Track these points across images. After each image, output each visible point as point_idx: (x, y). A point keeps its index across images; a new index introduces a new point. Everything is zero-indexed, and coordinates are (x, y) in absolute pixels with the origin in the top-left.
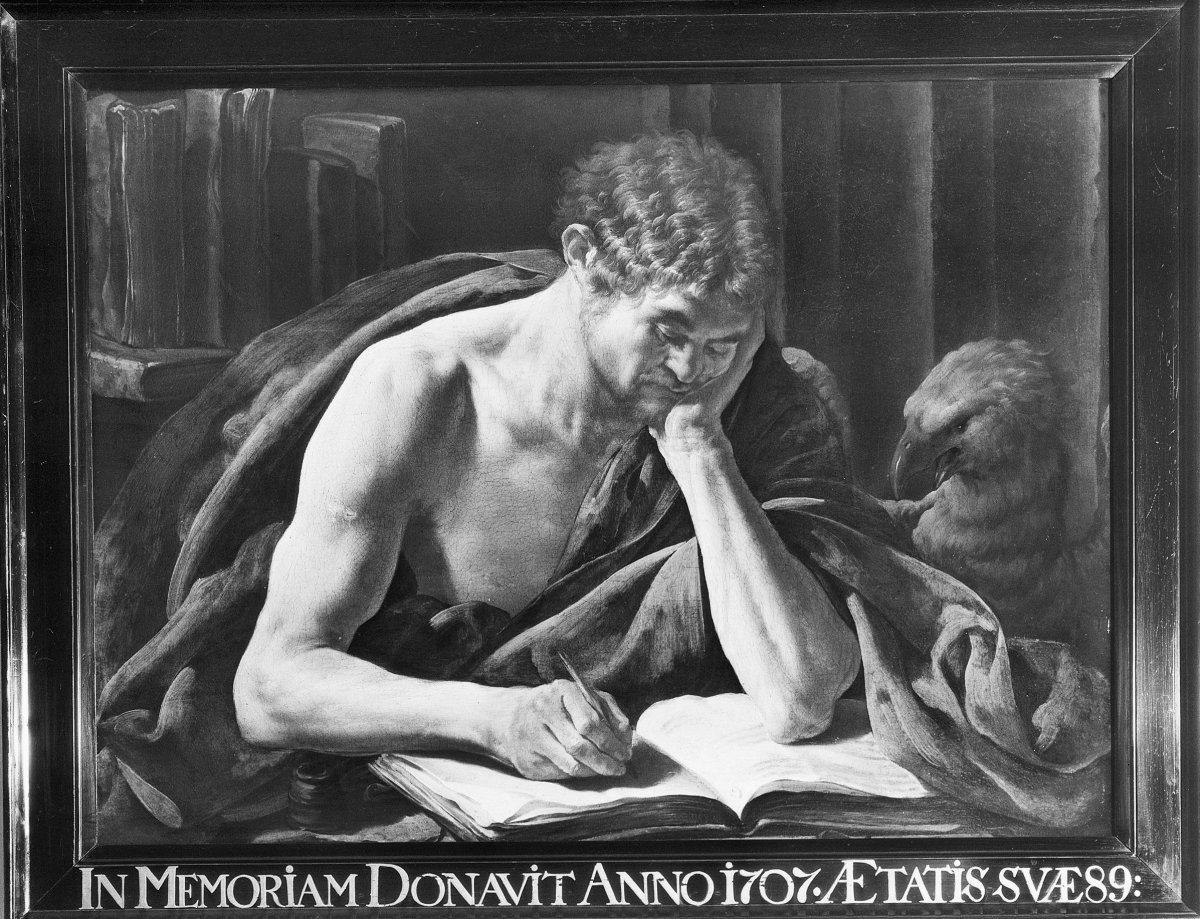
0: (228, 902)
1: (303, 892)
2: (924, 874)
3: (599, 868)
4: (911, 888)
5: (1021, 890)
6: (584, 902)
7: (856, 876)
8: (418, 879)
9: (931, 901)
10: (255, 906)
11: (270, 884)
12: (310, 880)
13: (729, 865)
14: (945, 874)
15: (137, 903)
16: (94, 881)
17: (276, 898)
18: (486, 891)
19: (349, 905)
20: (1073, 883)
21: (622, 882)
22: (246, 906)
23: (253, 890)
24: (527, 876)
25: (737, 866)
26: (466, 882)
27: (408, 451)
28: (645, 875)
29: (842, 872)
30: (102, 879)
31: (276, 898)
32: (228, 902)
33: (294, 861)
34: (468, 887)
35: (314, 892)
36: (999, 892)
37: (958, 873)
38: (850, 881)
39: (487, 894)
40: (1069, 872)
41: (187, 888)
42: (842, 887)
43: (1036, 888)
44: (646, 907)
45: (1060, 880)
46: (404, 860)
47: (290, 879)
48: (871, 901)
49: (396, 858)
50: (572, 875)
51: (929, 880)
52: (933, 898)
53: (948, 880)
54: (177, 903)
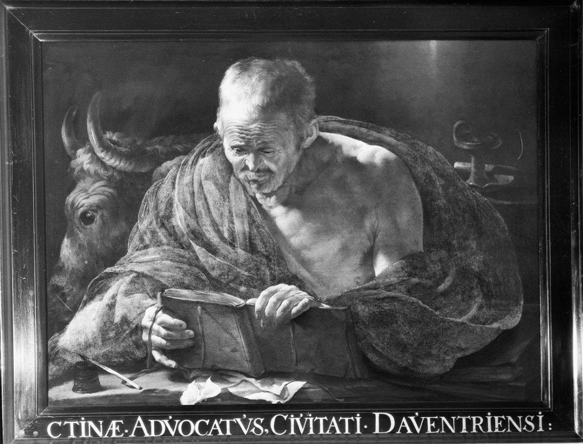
2: (220, 423)
3: (139, 419)
4: (331, 427)
6: (399, 432)
11: (478, 421)
13: (489, 414)
14: (75, 425)
15: (427, 431)
16: (87, 425)
17: (481, 428)
18: (401, 426)
19: (375, 433)
22: (186, 436)
23: (51, 429)
24: (307, 419)
25: (314, 416)
26: (98, 425)
27: (389, 256)
30: (91, 423)
31: (481, 428)
33: (85, 415)
34: (92, 430)
35: (143, 426)
36: (253, 430)
37: (83, 423)
39: (137, 428)
41: (499, 422)
42: (111, 432)
43: (91, 427)
44: (101, 439)
48: (438, 432)
50: (326, 418)
51: (223, 426)
53: (234, 426)
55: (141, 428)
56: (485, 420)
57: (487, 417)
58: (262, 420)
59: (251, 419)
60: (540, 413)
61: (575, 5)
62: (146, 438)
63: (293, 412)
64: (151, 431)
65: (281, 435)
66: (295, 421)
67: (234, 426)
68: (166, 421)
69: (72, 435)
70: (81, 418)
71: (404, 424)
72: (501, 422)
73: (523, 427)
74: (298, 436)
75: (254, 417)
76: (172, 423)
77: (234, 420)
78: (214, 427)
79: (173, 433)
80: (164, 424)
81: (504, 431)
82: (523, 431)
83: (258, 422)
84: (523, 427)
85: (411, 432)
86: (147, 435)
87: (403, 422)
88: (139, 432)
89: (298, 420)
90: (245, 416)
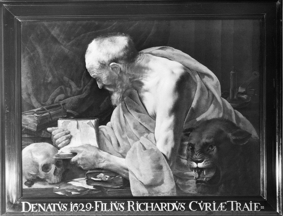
0: (139, 209)
1: (244, 207)
2: (51, 205)
4: (156, 208)
5: (124, 208)
7: (223, 206)
8: (141, 204)
9: (160, 210)
10: (30, 211)
11: (208, 205)
12: (157, 204)
13: (112, 202)
14: (56, 205)
17: (165, 209)
20: (257, 206)
21: (39, 206)
26: (43, 206)
28: (162, 204)
29: (220, 205)
31: (165, 209)
32: (139, 209)
34: (41, 208)
36: (180, 209)
38: (222, 207)
39: (48, 209)
40: (207, 204)
41: (98, 205)
42: (220, 208)
43: (61, 208)
45: (221, 205)
46: (30, 201)
47: (214, 204)
49: (133, 200)
52: (250, 210)
53: (57, 207)
54: (104, 209)
55: (247, 208)
56: (212, 205)
57: (71, 204)
58: (184, 204)
59: (179, 204)
60: (71, 202)
61: (278, 3)
62: (52, 212)
63: (72, 201)
64: (168, 209)
65: (143, 211)
66: (113, 205)
67: (57, 207)
68: (175, 204)
69: (24, 210)
70: (70, 202)
71: (156, 206)
72: (257, 206)
73: (119, 208)
74: (209, 212)
75: (120, 203)
76: (177, 205)
77: (144, 204)
78: (48, 207)
79: (177, 209)
80: (174, 205)
81: (36, 211)
82: (62, 211)
83: (183, 205)
84: (119, 208)
85: (130, 210)
86: (249, 210)
87: (49, 206)
88: (246, 209)
89: (115, 204)
90: (116, 202)
